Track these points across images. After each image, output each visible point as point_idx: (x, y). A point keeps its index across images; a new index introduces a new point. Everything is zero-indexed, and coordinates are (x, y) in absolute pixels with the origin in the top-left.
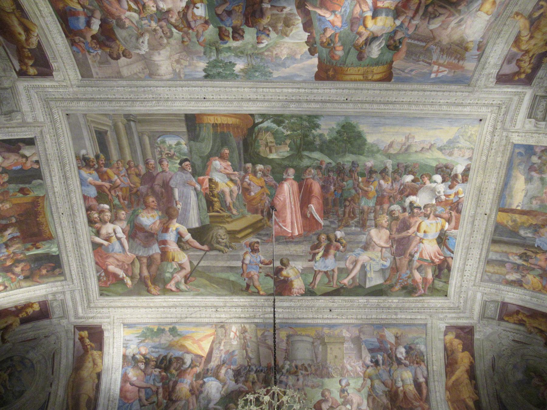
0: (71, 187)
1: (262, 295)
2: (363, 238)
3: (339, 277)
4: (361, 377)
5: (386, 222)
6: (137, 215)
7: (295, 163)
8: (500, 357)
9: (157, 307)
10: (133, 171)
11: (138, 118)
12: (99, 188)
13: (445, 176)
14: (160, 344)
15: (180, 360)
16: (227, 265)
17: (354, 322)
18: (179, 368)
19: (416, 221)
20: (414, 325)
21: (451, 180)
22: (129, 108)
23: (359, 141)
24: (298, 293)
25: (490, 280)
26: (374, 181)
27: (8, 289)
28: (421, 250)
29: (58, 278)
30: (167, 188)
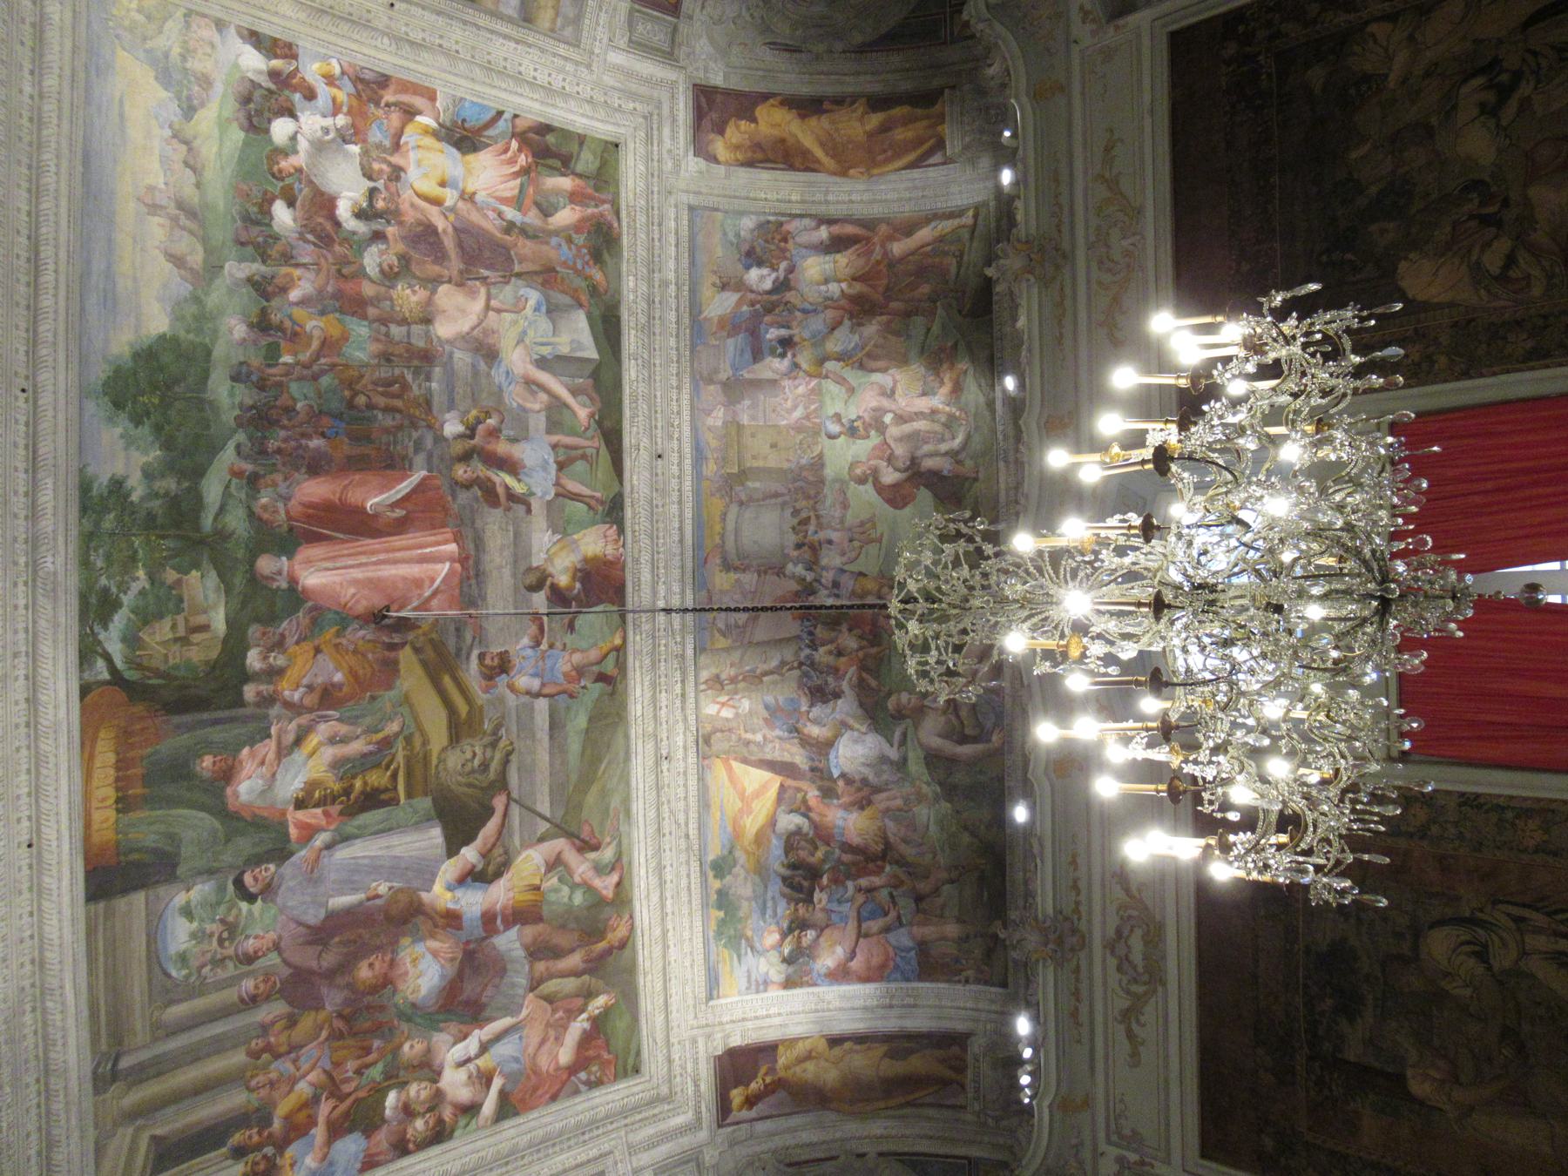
1: (624, 639)
2: (462, 358)
3: (573, 433)
4: (819, 384)
5: (414, 292)
6: (414, 1005)
7: (240, 554)
8: (766, 29)
10: (277, 1039)
11: (104, 1047)
12: (336, 1131)
13: (276, 107)
14: (755, 898)
15: (792, 841)
16: (546, 738)
17: (687, 397)
19: (412, 205)
21: (287, 92)
23: (167, 358)
24: (617, 541)
25: (577, 21)
26: (290, 317)
28: (491, 200)
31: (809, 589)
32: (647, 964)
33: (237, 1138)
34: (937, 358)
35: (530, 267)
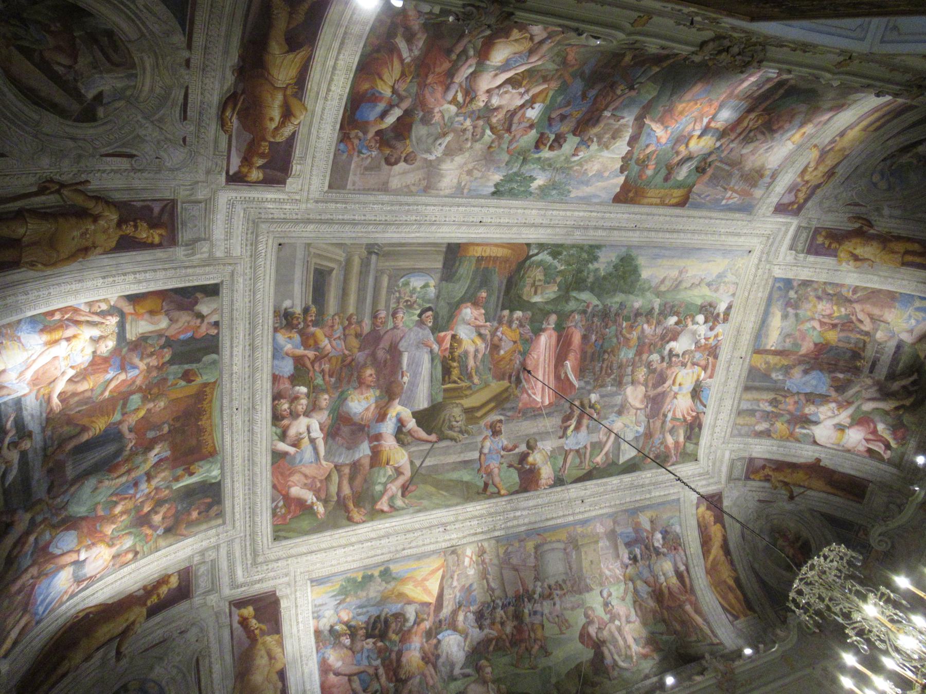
0: (258, 363)
1: (503, 496)
2: (618, 399)
3: (591, 455)
6: (346, 399)
9: (361, 542)
12: (298, 361)
14: (368, 600)
15: (400, 616)
18: (401, 629)
20: (668, 502)
22: (378, 235)
25: (740, 435)
27: (139, 556)
29: (213, 523)
30: (395, 352)
31: (530, 599)
32: (337, 536)
33: (313, 309)
34: (652, 641)
35: (651, 424)
